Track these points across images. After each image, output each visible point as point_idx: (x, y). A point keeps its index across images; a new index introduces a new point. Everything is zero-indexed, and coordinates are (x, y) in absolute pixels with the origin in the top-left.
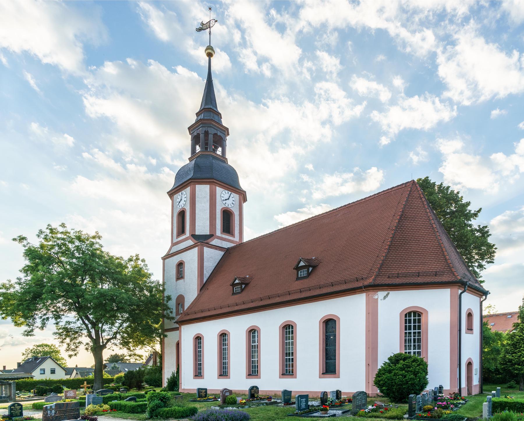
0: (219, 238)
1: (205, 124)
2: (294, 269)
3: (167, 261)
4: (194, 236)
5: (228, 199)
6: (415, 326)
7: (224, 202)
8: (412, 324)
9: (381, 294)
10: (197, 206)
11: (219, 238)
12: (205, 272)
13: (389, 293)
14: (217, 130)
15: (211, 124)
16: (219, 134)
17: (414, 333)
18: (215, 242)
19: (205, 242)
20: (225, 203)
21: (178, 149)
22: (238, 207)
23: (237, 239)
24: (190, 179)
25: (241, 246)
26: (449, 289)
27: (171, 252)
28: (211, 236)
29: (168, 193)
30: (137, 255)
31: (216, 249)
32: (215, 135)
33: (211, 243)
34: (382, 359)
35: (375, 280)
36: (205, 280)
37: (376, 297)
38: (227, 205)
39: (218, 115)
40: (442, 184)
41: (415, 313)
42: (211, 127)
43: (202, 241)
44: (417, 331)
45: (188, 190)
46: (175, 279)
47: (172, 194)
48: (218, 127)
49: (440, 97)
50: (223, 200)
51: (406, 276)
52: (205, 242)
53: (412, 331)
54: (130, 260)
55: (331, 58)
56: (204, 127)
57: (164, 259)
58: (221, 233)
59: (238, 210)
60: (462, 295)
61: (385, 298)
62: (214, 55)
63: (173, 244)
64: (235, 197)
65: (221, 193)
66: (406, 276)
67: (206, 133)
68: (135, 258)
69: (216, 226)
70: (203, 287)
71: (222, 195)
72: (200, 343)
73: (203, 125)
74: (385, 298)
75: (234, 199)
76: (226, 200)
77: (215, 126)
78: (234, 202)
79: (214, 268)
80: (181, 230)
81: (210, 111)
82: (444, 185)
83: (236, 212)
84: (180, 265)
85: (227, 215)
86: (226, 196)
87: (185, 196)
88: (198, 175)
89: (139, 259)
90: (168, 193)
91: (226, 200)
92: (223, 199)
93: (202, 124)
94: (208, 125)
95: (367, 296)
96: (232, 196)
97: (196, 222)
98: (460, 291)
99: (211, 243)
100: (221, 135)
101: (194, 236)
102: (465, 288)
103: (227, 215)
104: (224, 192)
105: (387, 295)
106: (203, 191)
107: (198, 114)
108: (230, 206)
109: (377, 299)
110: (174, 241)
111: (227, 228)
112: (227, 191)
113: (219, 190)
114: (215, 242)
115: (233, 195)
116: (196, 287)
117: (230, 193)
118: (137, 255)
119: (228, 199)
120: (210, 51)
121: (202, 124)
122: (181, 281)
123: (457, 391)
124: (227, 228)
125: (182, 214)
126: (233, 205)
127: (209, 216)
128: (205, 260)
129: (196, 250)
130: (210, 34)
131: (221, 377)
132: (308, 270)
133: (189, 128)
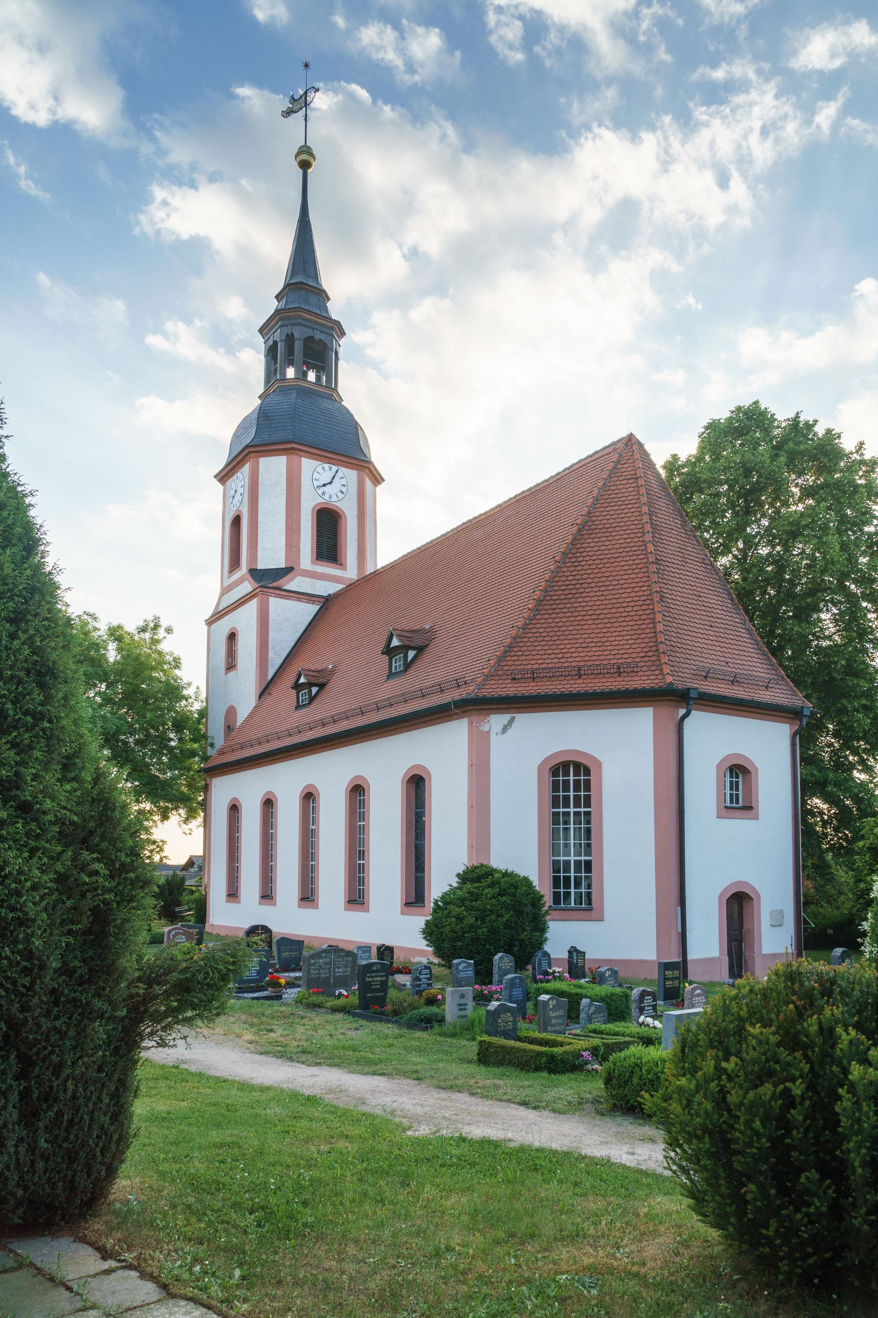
0: (307, 574)
1: (288, 318)
2: (383, 653)
3: (213, 626)
4: (254, 573)
5: (330, 483)
6: (577, 799)
7: (320, 491)
8: (572, 794)
9: (496, 721)
10: (260, 504)
11: (307, 574)
12: (271, 654)
13: (513, 719)
14: (313, 329)
15: (300, 317)
16: (318, 336)
17: (576, 814)
18: (295, 584)
19: (274, 585)
20: (324, 493)
21: (240, 381)
22: (355, 499)
23: (351, 572)
24: (247, 446)
25: (371, 583)
26: (651, 709)
28: (288, 571)
29: (216, 477)
30: (157, 618)
31: (299, 600)
32: (309, 340)
33: (285, 588)
34: (441, 880)
35: (481, 686)
36: (271, 672)
37: (486, 728)
38: (327, 497)
39: (316, 293)
40: (797, 416)
41: (578, 766)
42: (299, 324)
43: (268, 581)
44: (582, 810)
45: (246, 469)
46: (224, 670)
47: (224, 477)
48: (316, 322)
49: (669, 238)
50: (318, 487)
51: (552, 674)
53: (572, 810)
54: (143, 630)
56: (286, 326)
57: (210, 622)
58: (313, 563)
59: (355, 505)
60: (687, 722)
61: (505, 729)
62: (314, 164)
63: (225, 591)
64: (349, 475)
65: (314, 471)
66: (552, 674)
67: (290, 340)
68: (152, 625)
69: (299, 549)
70: (265, 690)
71: (316, 475)
72: (363, 804)
73: (285, 322)
74: (505, 729)
75: (344, 481)
76: (324, 485)
77: (309, 320)
78: (344, 489)
79: (293, 644)
80: (235, 562)
81: (301, 289)
82: (802, 418)
83: (348, 509)
84: (232, 637)
85: (328, 521)
86: (326, 477)
87: (242, 483)
88: (265, 437)
89: (160, 626)
90: (216, 477)
91: (324, 485)
92: (316, 483)
93: (281, 319)
94: (292, 322)
95: (471, 723)
96: (340, 474)
98: (682, 712)
99: (288, 587)
100: (323, 337)
101: (254, 573)
102: (688, 704)
103: (328, 521)
104: (319, 469)
105: (510, 722)
106: (273, 468)
107: (278, 297)
108: (334, 499)
109: (489, 732)
110: (225, 585)
111: (329, 546)
112: (326, 466)
113: (308, 465)
114: (295, 584)
115: (344, 471)
116: (254, 687)
117: (334, 468)
118: (157, 618)
119: (330, 483)
120: (304, 157)
121: (281, 319)
122: (232, 674)
123: (676, 958)
124: (329, 546)
125: (237, 521)
126: (341, 496)
127: (284, 525)
128: (272, 625)
129: (254, 604)
130: (306, 120)
131: (264, 901)
132: (406, 656)
133: (259, 331)
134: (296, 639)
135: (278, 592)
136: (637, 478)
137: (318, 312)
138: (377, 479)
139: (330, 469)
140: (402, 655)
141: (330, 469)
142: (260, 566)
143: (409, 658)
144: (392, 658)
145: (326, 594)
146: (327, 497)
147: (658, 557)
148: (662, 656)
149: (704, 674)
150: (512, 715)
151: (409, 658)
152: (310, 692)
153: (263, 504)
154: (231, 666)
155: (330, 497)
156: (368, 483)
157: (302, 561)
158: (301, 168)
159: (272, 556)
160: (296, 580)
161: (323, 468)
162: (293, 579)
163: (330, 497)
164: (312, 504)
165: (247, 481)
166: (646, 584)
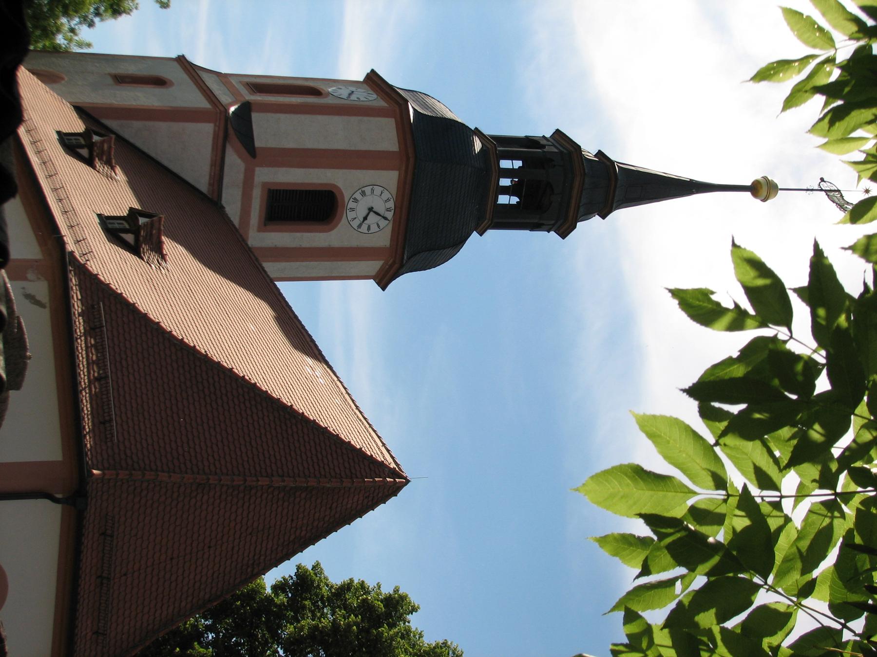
0: (249, 177)
3: (175, 64)
11: (249, 177)
13: (42, 306)
18: (234, 161)
19: (231, 131)
20: (369, 228)
23: (259, 238)
27: (204, 76)
29: (373, 71)
31: (213, 164)
37: (30, 276)
38: (351, 205)
45: (382, 103)
46: (114, 72)
47: (373, 79)
50: (360, 226)
52: (231, 131)
55: (600, 154)
58: (264, 184)
60: (47, 502)
64: (380, 234)
76: (365, 218)
79: (153, 155)
85: (320, 207)
90: (373, 71)
91: (365, 218)
96: (383, 223)
97: (288, 116)
103: (320, 207)
104: (386, 195)
106: (384, 136)
108: (351, 215)
109: (26, 279)
112: (391, 204)
114: (234, 161)
116: (88, 100)
117: (390, 215)
122: (110, 81)
134: (159, 159)
135: (221, 134)
136: (351, 478)
137: (583, 201)
138: (384, 281)
139: (388, 210)
140: (127, 226)
141: (388, 210)
142: (255, 116)
143: (124, 236)
144: (126, 221)
145: (224, 202)
146: (351, 205)
147: (253, 491)
148: (127, 472)
149: (109, 532)
150: (48, 305)
151: (124, 236)
152: (82, 147)
153: (337, 122)
154: (121, 80)
155: (352, 210)
156: (375, 266)
157: (265, 170)
158: (753, 183)
159: (267, 130)
160: (239, 161)
161: (388, 200)
162: (240, 157)
163: (352, 210)
164: (340, 185)
165: (367, 103)
166: (218, 471)
